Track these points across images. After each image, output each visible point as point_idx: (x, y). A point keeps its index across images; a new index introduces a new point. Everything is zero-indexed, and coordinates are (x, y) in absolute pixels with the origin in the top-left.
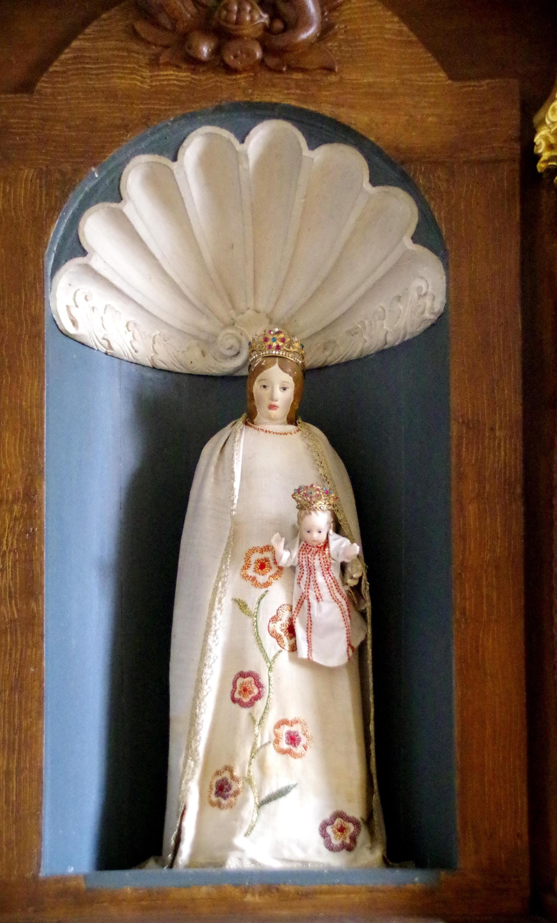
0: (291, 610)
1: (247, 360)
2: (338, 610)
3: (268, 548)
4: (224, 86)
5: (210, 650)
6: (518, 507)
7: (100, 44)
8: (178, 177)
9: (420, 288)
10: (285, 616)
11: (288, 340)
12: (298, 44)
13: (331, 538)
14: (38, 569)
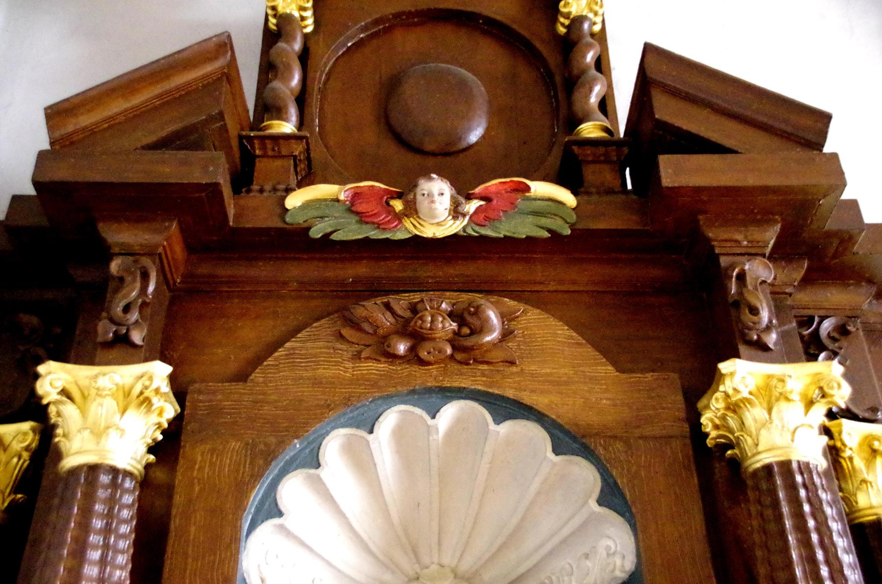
4: (418, 375)
7: (309, 345)
8: (374, 446)
9: (608, 548)
12: (482, 344)
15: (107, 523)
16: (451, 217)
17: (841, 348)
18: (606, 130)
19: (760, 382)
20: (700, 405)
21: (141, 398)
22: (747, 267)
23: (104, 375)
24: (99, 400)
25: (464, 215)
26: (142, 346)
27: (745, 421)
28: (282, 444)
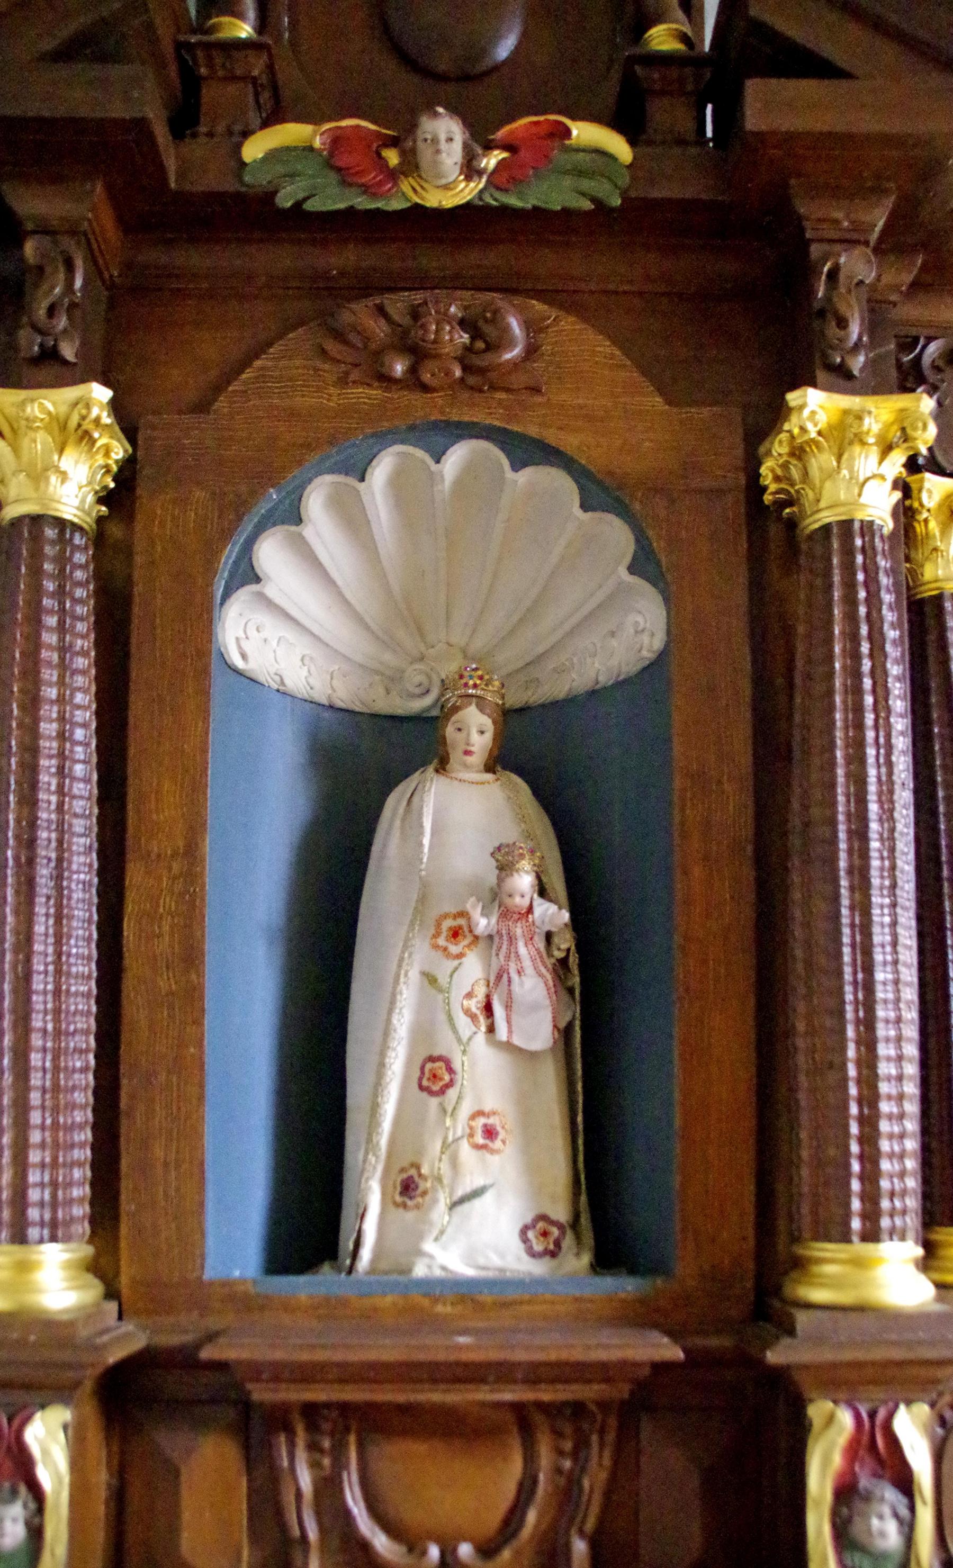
0: (488, 985)
1: (438, 700)
2: (542, 985)
3: (463, 914)
5: (395, 1030)
6: (748, 873)
7: (282, 363)
8: (366, 499)
10: (481, 992)
11: (486, 677)
12: (501, 364)
13: (535, 904)
14: (199, 933)
15: (59, 586)
16: (462, 177)
17: (943, 381)
18: (684, 38)
19: (835, 419)
20: (762, 450)
21: (80, 432)
22: (842, 260)
23: (33, 401)
24: (31, 434)
25: (480, 173)
26: (75, 364)
27: (809, 469)
28: (255, 494)
